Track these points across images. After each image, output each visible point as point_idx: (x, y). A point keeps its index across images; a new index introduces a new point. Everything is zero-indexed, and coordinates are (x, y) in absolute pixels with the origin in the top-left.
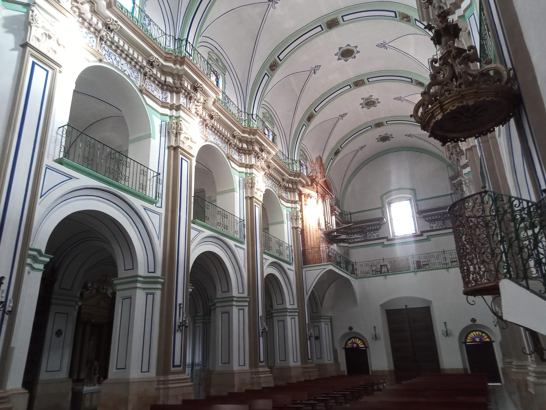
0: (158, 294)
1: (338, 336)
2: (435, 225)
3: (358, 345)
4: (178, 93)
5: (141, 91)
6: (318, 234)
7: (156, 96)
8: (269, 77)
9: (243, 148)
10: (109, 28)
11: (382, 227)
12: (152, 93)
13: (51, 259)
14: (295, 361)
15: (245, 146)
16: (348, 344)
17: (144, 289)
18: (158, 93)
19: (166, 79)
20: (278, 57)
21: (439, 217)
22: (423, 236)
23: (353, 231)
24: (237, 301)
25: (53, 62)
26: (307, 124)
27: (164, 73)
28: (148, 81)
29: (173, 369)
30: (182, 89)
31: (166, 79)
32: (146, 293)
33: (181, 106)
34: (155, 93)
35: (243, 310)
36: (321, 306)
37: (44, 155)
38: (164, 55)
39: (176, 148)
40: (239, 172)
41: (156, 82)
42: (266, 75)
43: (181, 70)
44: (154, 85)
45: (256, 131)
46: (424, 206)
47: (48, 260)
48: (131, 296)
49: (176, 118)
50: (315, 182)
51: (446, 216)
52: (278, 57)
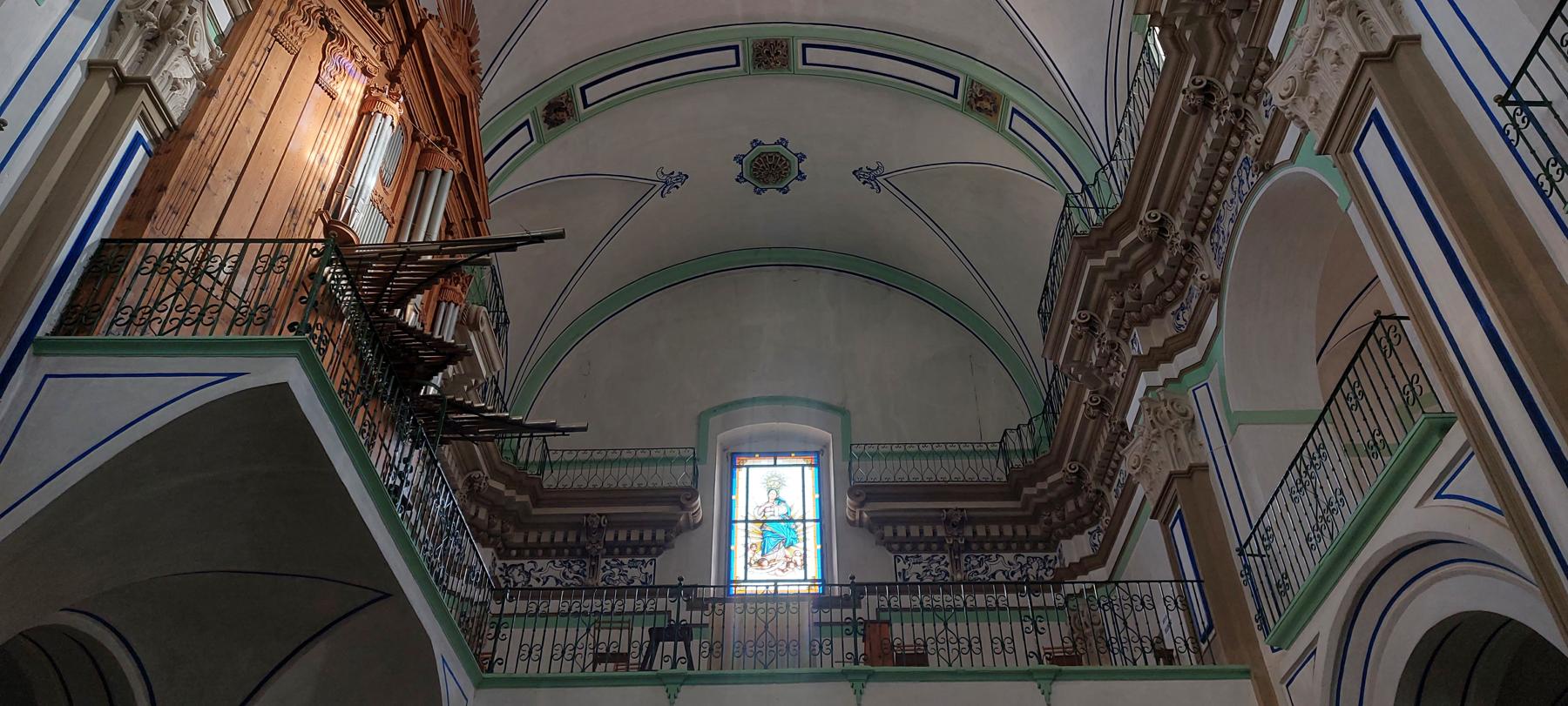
2: (919, 568)
11: (678, 541)
21: (941, 533)
22: (670, 611)
39: (123, 84)
46: (876, 472)
51: (968, 532)
52: (583, 90)
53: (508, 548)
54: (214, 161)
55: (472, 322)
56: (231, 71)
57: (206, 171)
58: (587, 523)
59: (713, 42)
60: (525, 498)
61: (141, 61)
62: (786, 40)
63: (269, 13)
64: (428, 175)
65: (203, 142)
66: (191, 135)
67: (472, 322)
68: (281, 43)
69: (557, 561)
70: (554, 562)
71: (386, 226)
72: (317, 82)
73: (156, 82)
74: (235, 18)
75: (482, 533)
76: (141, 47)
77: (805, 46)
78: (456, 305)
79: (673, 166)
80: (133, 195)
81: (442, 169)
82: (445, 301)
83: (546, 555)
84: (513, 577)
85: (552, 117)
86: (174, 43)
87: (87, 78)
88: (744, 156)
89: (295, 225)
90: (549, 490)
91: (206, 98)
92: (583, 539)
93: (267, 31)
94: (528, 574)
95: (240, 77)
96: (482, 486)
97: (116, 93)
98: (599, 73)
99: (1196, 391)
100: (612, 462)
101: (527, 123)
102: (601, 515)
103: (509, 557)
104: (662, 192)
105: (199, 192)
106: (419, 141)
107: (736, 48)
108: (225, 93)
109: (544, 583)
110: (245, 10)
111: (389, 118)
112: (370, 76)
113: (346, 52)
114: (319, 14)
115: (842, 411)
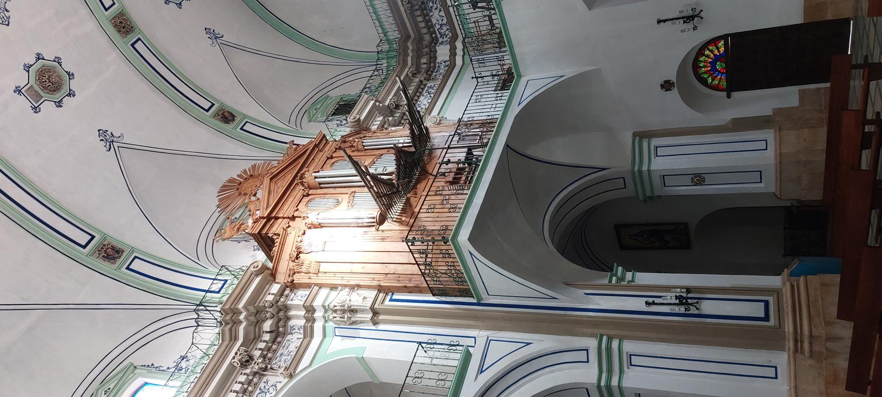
0: (630, 346)
1: (687, 116)
3: (717, 58)
4: (286, 308)
5: (291, 376)
7: (298, 345)
8: (247, 122)
9: (428, 62)
10: (247, 361)
12: (293, 354)
13: (618, 266)
14: (771, 372)
15: (267, 325)
16: (716, 82)
17: (621, 372)
18: (294, 341)
19: (267, 332)
20: (207, 111)
23: (425, 31)
24: (610, 371)
25: (376, 300)
26: (241, 122)
27: (257, 338)
28: (274, 362)
29: (772, 322)
30: (279, 303)
31: (267, 332)
32: (628, 368)
33: (305, 305)
34: (293, 348)
35: (656, 148)
36: (604, 169)
38: (226, 343)
39: (375, 313)
40: (324, 336)
41: (274, 347)
42: (130, 267)
43: (248, 310)
44: (281, 351)
45: (229, 311)
47: (620, 268)
48: (660, 176)
49: (326, 311)
50: (264, 232)
52: (207, 111)
53: (433, 39)
55: (358, 123)
57: (389, 276)
58: (409, 10)
59: (153, 73)
60: (409, 44)
61: (363, 311)
62: (111, 21)
63: (310, 278)
64: (320, 184)
65: (379, 281)
66: (380, 286)
67: (358, 123)
69: (431, 14)
70: (432, 16)
71: (356, 195)
72: (324, 251)
73: (369, 305)
75: (432, 56)
76: (358, 313)
77: (106, 10)
78: (363, 142)
79: (206, 41)
80: (411, 293)
83: (430, 21)
84: (445, 32)
85: (230, 118)
86: (351, 306)
87: (379, 323)
88: (176, 4)
90: (400, 33)
92: (417, 7)
94: (441, 25)
95: (344, 278)
96: (414, 69)
97: (379, 313)
98: (194, 107)
99: (632, 364)
100: (374, 8)
101: (242, 129)
102: (403, 5)
103: (436, 37)
104: (221, 37)
106: (308, 193)
107: (133, 45)
109: (443, 17)
110: (315, 287)
112: (305, 231)
114: (296, 261)
115: (136, 257)
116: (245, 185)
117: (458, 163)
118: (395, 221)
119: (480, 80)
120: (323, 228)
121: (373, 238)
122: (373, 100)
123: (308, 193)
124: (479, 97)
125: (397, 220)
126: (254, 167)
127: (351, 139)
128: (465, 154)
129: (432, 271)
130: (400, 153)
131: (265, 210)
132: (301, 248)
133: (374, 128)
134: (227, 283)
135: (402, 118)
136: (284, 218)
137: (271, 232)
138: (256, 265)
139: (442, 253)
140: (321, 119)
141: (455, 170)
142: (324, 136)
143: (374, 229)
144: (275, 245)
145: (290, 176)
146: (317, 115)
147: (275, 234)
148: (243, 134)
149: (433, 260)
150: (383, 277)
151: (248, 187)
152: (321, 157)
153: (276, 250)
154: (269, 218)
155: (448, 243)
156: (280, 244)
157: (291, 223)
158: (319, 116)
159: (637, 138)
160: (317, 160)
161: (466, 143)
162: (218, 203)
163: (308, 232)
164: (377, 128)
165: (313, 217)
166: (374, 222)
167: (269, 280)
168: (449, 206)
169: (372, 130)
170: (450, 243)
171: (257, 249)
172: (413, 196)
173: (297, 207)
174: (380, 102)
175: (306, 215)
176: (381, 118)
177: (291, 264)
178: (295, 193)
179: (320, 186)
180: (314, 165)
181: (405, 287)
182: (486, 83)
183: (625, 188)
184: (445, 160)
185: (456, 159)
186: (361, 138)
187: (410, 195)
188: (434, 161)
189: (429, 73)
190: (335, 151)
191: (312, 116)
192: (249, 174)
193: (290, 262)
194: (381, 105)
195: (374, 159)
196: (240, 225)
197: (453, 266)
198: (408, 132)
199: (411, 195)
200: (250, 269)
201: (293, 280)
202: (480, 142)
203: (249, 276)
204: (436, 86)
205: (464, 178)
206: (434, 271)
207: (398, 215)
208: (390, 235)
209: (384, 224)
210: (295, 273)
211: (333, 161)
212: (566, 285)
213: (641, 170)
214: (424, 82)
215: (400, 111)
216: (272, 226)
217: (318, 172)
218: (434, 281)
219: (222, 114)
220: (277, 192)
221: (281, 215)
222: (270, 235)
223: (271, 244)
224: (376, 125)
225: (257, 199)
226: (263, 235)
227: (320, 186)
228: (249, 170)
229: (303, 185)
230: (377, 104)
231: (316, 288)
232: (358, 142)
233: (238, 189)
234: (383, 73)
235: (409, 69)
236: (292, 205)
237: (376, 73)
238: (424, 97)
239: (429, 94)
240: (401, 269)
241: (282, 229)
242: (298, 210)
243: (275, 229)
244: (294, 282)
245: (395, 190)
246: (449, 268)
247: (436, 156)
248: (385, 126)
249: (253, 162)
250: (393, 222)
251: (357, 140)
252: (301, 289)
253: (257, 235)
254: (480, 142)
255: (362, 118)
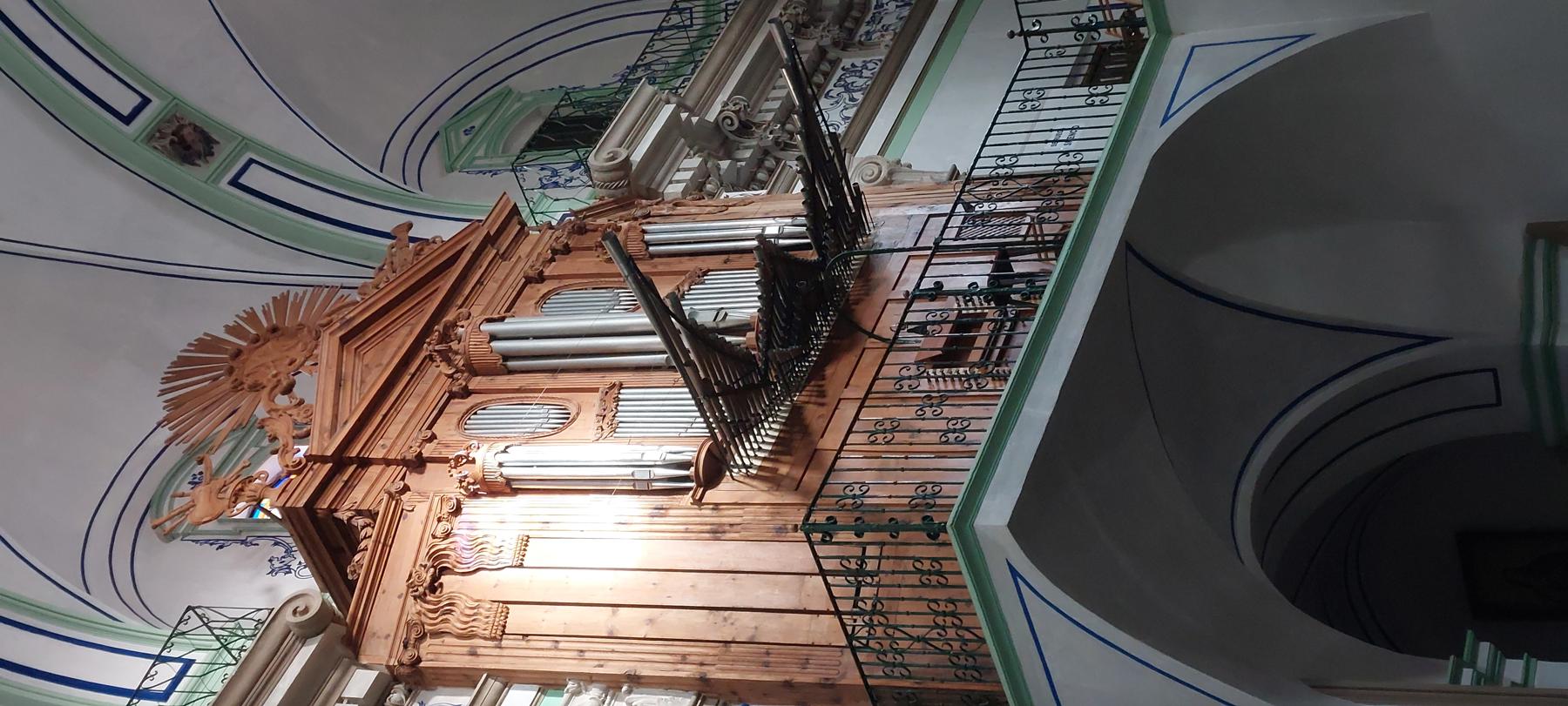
6: (746, 515)
8: (251, 161)
13: (1480, 638)
36: (1427, 340)
37: (1121, 177)
42: (241, 181)
47: (1485, 648)
52: (127, 120)
54: (717, 645)
55: (621, 173)
56: (588, 668)
57: (734, 648)
64: (506, 357)
65: (702, 664)
67: (621, 173)
68: (504, 627)
71: (624, 392)
72: (521, 566)
74: (507, 685)
78: (644, 232)
81: (489, 342)
82: (648, 248)
85: (199, 147)
89: (731, 525)
91: (643, 681)
93: (500, 648)
95: (587, 655)
96: (800, 10)
101: (234, 183)
105: (766, 646)
108: (621, 664)
110: (491, 681)
111: (502, 458)
112: (459, 502)
113: (452, 546)
114: (428, 598)
116: (256, 359)
117: (969, 293)
118: (755, 477)
119: (1034, 41)
120: (521, 498)
121: (682, 528)
122: (668, 102)
123: (466, 386)
124: (1034, 95)
125: (761, 473)
126: (280, 303)
127: (603, 221)
128: (988, 269)
129: (879, 631)
130: (772, 258)
131: (326, 435)
132: (447, 556)
133: (673, 190)
134: (193, 670)
135: (760, 164)
136: (387, 462)
137: (347, 505)
138: (301, 604)
139: (919, 571)
140: (487, 161)
141: (953, 316)
142: (515, 211)
143: (687, 499)
144: (362, 545)
145: (404, 331)
146: (477, 149)
147: (359, 513)
148: (238, 198)
149: (883, 593)
150: (712, 651)
151: (267, 362)
152: (507, 276)
153: (365, 562)
154: (339, 461)
155: (942, 537)
156: (377, 542)
157: (412, 480)
158: (481, 153)
159: (1541, 245)
160: (491, 286)
161: (994, 233)
162: (165, 413)
163: (470, 506)
164: (685, 192)
165: (486, 458)
166: (686, 479)
167: (340, 659)
168: (942, 425)
169: (670, 199)
170: (951, 536)
171: (281, 569)
172: (813, 399)
173: (430, 427)
174: (691, 111)
175: (463, 453)
176: (696, 161)
177: (413, 607)
178: (422, 387)
179: (504, 365)
180: (483, 300)
181: (788, 685)
182: (1054, 52)
183: (1499, 403)
184: (927, 284)
185: (963, 284)
186: (636, 219)
187: (802, 398)
188: (880, 296)
189: (847, 24)
190: (552, 260)
191: (456, 152)
192: (265, 324)
193: (411, 600)
194: (695, 120)
195: (682, 284)
196: (243, 482)
197: (953, 614)
198: (798, 205)
199: (806, 399)
200: (280, 618)
201: (419, 660)
202: (1031, 232)
203: (279, 640)
204: (870, 66)
205: (981, 342)
206: (890, 631)
207: (764, 459)
208: (738, 520)
209: (721, 486)
210: (424, 636)
211: (544, 288)
212: (1313, 687)
213: (1553, 345)
214: (832, 54)
215: (754, 143)
216: (348, 486)
217: (502, 319)
218: (887, 664)
219: (173, 134)
220: (362, 382)
221: (378, 453)
222: (343, 515)
223: (343, 544)
224: (678, 182)
225: (295, 402)
226: (320, 514)
227: (504, 365)
228: (264, 312)
229: (449, 362)
230: (684, 115)
231: (494, 685)
232: (628, 230)
233: (231, 371)
234: (691, 18)
235: (785, 8)
236: (414, 422)
237: (675, 19)
238: (832, 101)
239: (847, 90)
240: (772, 629)
241: (386, 497)
242: (434, 437)
243: (357, 496)
244: (422, 665)
245: (756, 379)
246: (940, 620)
247: (885, 279)
248: (709, 187)
249: (277, 291)
250: (747, 481)
251: (624, 225)
252: (440, 689)
253: (304, 513)
254: (1031, 232)
255: (637, 157)
